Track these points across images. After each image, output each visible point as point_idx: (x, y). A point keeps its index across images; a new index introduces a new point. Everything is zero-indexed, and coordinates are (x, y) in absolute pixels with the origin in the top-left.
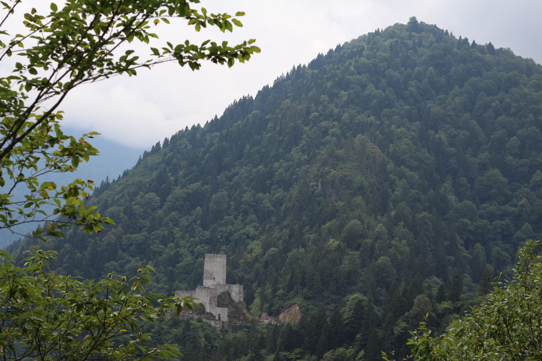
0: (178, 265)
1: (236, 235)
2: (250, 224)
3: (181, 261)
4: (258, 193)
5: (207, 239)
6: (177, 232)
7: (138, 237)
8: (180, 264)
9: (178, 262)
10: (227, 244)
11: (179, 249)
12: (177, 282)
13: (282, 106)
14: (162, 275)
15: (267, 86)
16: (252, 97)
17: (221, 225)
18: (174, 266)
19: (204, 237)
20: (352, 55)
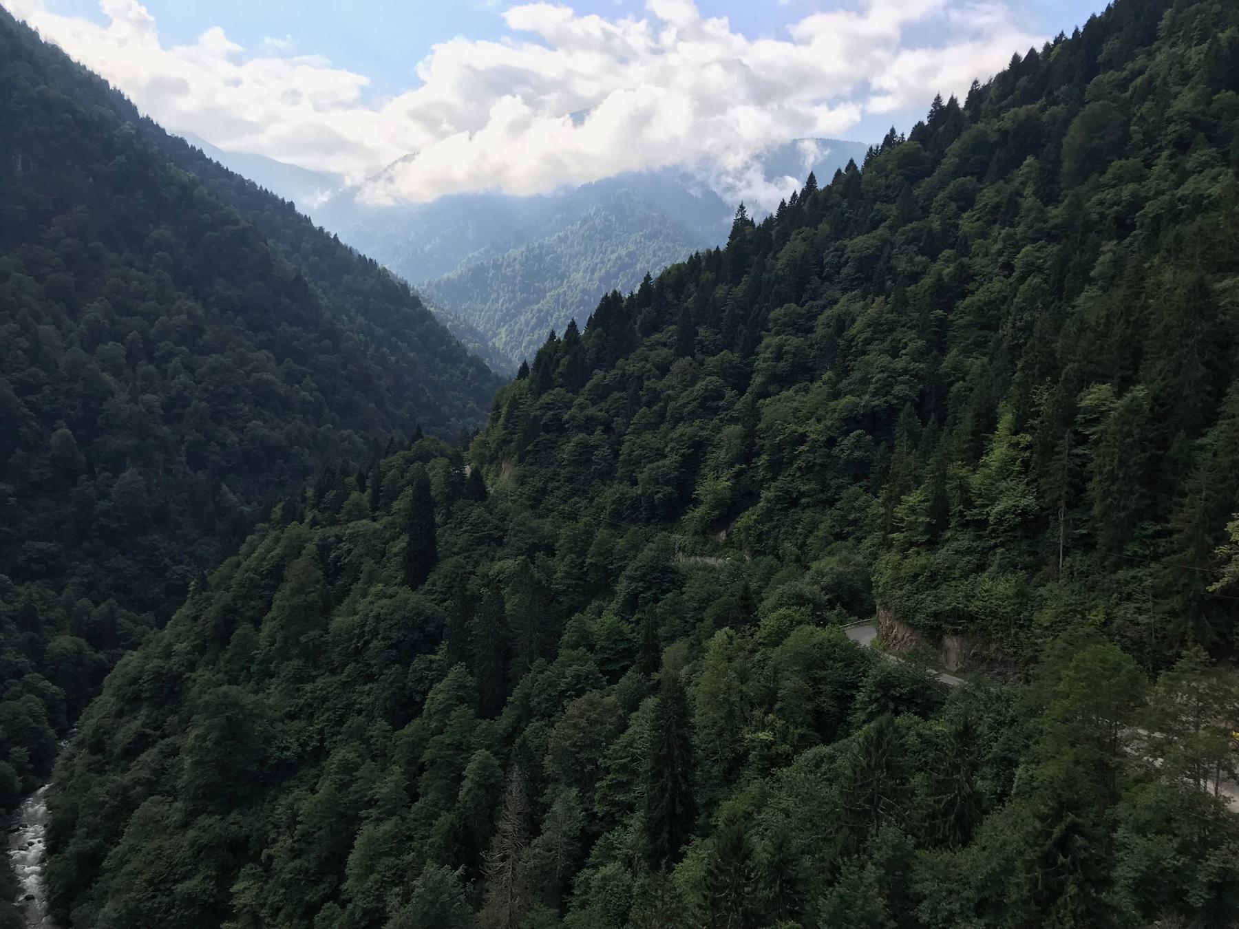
0: (962, 304)
1: (1150, 208)
2: (1200, 172)
3: (972, 292)
4: (1217, 92)
5: (1055, 227)
6: (967, 223)
7: (861, 243)
8: (968, 300)
9: (964, 295)
10: (1121, 238)
11: (965, 260)
12: (954, 352)
13: (259, 654)
14: (912, 334)
15: (921, 124)
16: (953, 101)
17: (1098, 188)
18: (949, 308)
19: (1045, 222)
20: (807, 279)
